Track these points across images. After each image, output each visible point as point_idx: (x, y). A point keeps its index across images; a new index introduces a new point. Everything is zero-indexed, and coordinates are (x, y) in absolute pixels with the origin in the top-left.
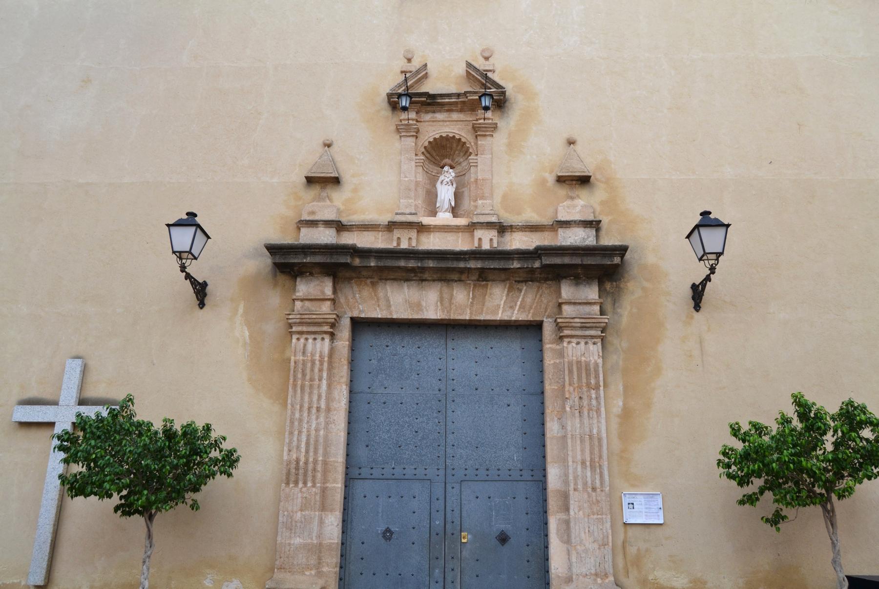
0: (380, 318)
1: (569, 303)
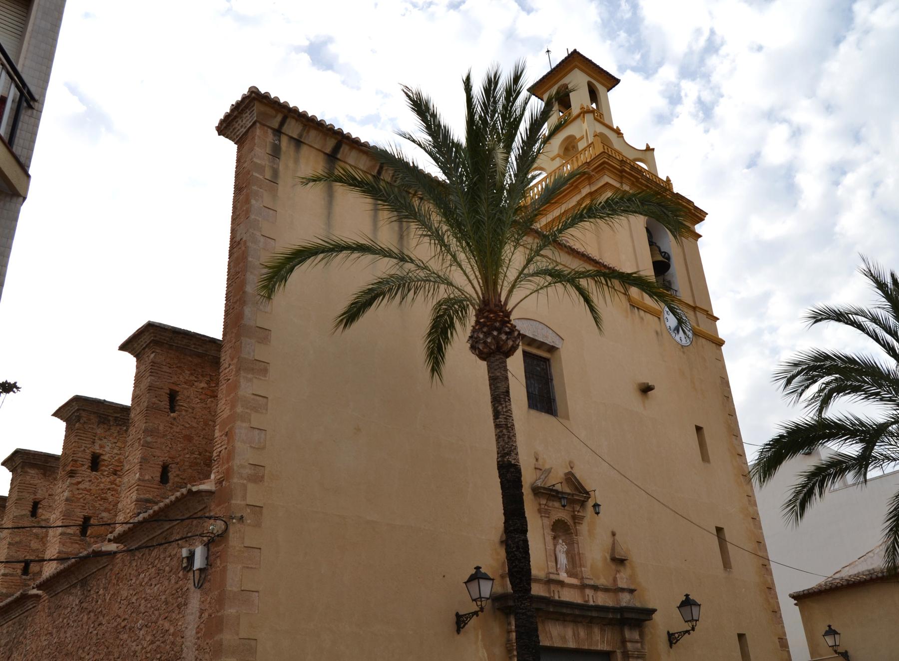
0: (549, 647)
1: (631, 641)
